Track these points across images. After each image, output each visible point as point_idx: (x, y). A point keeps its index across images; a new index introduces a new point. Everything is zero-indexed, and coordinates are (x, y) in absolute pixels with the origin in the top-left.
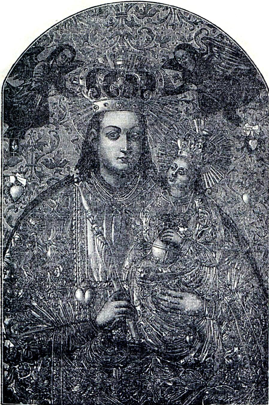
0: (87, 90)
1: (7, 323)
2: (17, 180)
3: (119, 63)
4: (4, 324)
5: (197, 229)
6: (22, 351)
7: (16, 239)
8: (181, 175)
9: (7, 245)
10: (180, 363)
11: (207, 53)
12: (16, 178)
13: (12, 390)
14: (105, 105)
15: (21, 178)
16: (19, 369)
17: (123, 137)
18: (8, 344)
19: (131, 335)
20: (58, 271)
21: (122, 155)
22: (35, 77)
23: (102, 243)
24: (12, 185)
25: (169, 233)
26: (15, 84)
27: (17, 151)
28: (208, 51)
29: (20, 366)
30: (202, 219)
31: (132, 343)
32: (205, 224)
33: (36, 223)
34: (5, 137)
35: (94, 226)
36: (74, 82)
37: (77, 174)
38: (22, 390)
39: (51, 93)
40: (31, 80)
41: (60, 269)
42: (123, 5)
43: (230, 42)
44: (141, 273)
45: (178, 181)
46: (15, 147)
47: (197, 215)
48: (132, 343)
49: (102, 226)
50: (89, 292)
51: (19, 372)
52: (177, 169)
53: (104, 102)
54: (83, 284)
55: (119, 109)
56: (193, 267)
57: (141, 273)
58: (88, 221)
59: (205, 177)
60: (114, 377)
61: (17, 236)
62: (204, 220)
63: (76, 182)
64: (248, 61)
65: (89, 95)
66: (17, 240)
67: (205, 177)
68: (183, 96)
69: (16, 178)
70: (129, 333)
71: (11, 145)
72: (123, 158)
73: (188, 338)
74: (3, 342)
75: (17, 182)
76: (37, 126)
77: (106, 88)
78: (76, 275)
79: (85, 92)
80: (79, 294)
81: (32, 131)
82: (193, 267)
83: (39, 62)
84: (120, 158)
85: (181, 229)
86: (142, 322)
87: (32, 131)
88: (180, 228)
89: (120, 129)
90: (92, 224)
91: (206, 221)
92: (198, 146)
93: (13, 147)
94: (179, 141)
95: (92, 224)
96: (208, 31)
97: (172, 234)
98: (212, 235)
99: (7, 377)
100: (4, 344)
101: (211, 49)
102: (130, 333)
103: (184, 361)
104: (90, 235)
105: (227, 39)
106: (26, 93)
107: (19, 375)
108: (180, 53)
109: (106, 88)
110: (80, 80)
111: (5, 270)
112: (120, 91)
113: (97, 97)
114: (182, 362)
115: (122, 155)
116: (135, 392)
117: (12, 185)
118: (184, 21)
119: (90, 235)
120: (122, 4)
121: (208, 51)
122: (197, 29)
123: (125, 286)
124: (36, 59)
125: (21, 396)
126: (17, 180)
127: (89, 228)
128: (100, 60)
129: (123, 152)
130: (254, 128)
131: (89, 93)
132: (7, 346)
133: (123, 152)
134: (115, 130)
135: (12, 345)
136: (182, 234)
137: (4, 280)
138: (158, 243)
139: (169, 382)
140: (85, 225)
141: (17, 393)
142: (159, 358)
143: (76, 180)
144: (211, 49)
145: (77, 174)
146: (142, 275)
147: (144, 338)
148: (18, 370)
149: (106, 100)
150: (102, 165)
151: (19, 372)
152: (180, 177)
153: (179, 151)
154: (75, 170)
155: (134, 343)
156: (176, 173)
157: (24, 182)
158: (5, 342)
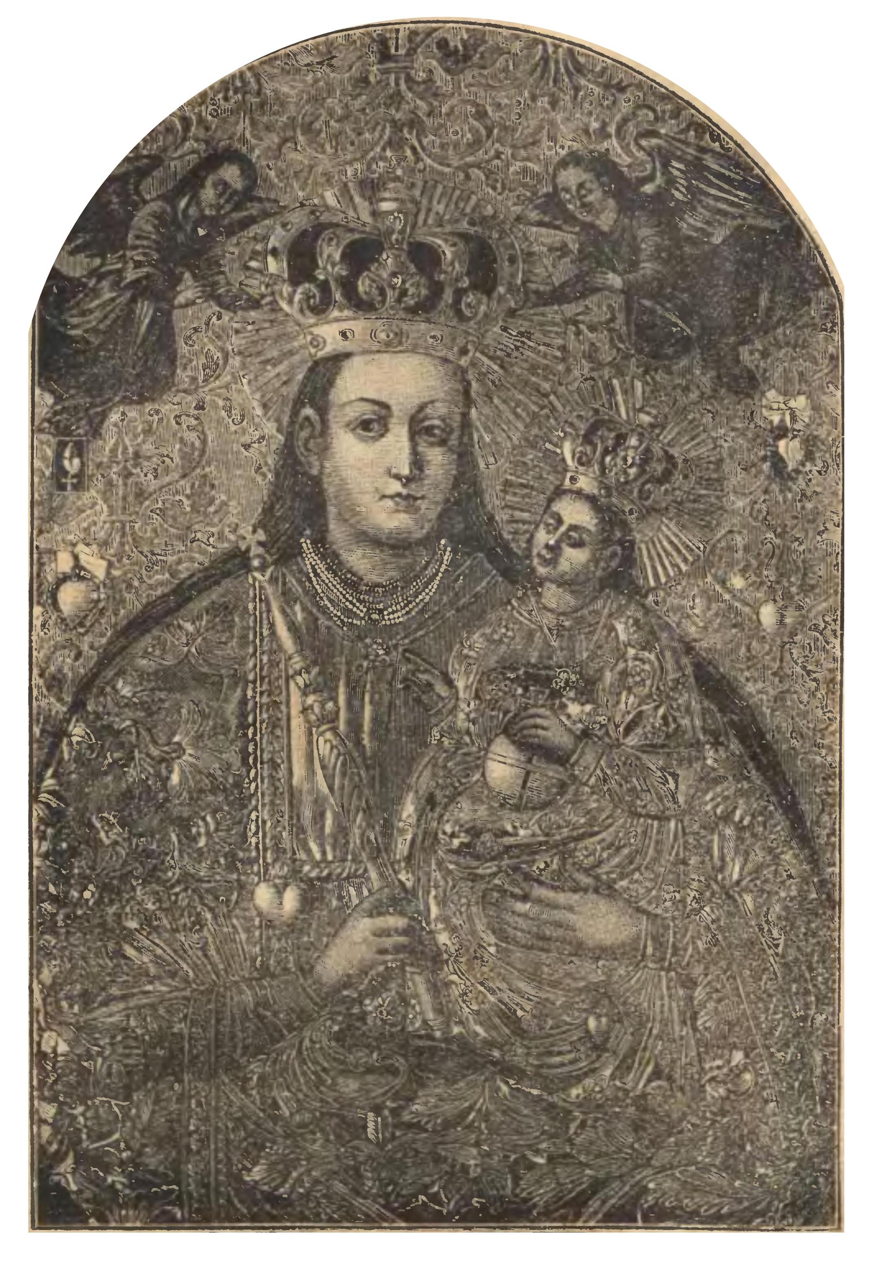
1: (48, 981)
3: (385, 206)
4: (40, 982)
7: (75, 739)
12: (76, 558)
13: (63, 1181)
14: (344, 334)
15: (92, 560)
16: (86, 1119)
18: (53, 1044)
19: (422, 1013)
20: (202, 830)
21: (396, 487)
22: (135, 247)
24: (64, 579)
25: (539, 721)
26: (77, 269)
27: (80, 475)
29: (88, 1108)
31: (420, 1037)
32: (647, 690)
34: (41, 430)
35: (310, 700)
36: (253, 264)
37: (260, 543)
38: (97, 1182)
39: (181, 299)
40: (124, 256)
41: (207, 824)
43: (722, 146)
44: (453, 835)
45: (564, 565)
46: (72, 465)
47: (621, 666)
48: (420, 1037)
49: (335, 700)
50: (298, 892)
51: (86, 1126)
52: (563, 529)
53: (344, 326)
54: (277, 866)
55: (388, 347)
56: (610, 821)
57: (453, 835)
58: (292, 685)
59: (645, 552)
61: (78, 730)
62: (643, 680)
63: (256, 569)
65: (296, 305)
69: (76, 558)
70: (414, 1007)
71: (59, 456)
72: (399, 495)
74: (36, 1038)
75: (78, 573)
76: (174, 723)
77: (348, 286)
78: (257, 844)
80: (263, 895)
83: (145, 202)
84: (392, 497)
85: (574, 709)
86: (454, 978)
87: (123, 414)
88: (569, 703)
89: (386, 406)
90: (305, 694)
91: (648, 682)
93: (66, 463)
95: (305, 694)
96: (654, 111)
97: (545, 723)
98: (666, 724)
99: (50, 1143)
100: (39, 1044)
102: (418, 1008)
105: (715, 138)
106: (108, 296)
107: (84, 1136)
108: (571, 177)
109: (348, 286)
110: (270, 259)
111: (42, 828)
112: (389, 293)
114: (575, 1092)
115: (396, 487)
116: (433, 1183)
117: (64, 579)
120: (397, 31)
121: (654, 169)
123: (403, 877)
125: (95, 1200)
126: (77, 565)
128: (330, 197)
129: (397, 477)
131: (297, 297)
132: (49, 1051)
133: (397, 477)
135: (63, 1048)
136: (574, 723)
137: (39, 856)
138: (502, 747)
139: (537, 1152)
140: (283, 697)
141: (80, 1192)
143: (256, 563)
145: (260, 543)
147: (461, 1023)
148: (81, 1119)
149: (348, 319)
151: (86, 1126)
154: (254, 531)
155: (431, 1037)
156: (558, 542)
157: (97, 567)
158: (41, 1036)
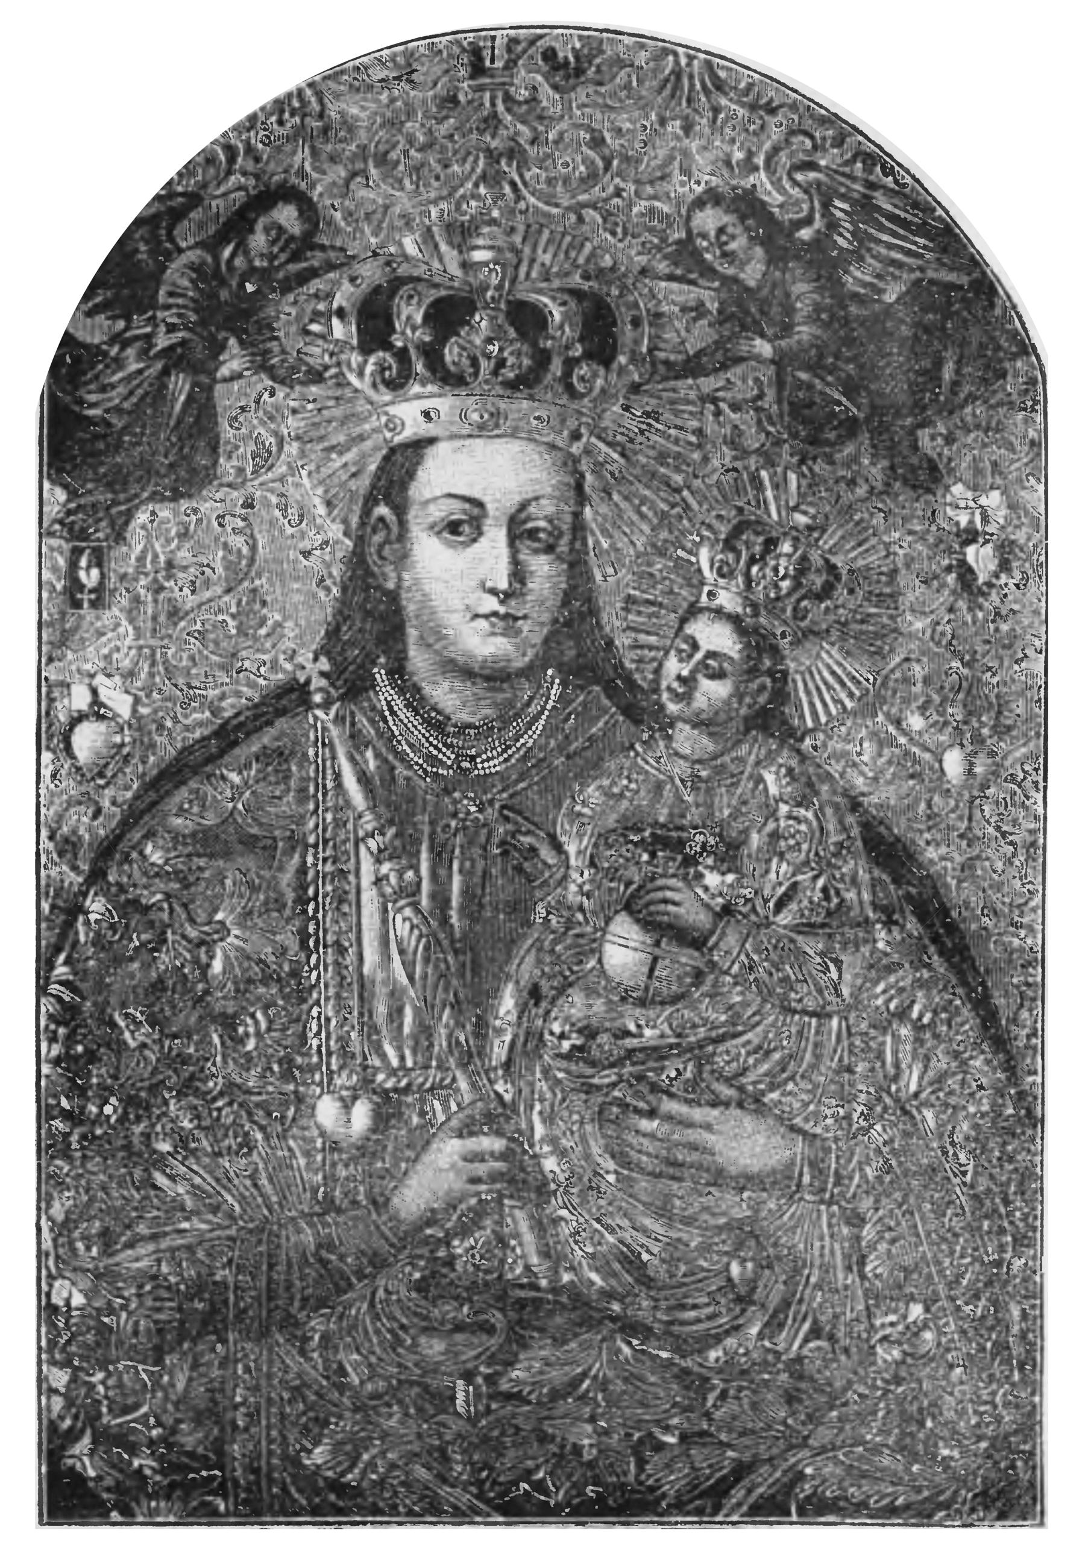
0: (360, 359)
1: (60, 1218)
2: (96, 700)
3: (479, 256)
5: (773, 876)
6: (119, 1317)
8: (712, 677)
9: (63, 936)
10: (706, 1359)
11: (808, 221)
12: (94, 692)
13: (78, 1465)
14: (427, 414)
15: (114, 694)
16: (107, 1388)
17: (495, 539)
18: (65, 1295)
19: (523, 1256)
20: (251, 1030)
21: (491, 604)
22: (168, 307)
23: (416, 932)
24: (79, 719)
26: (95, 334)
27: (99, 589)
28: (812, 209)
30: (792, 842)
33: (168, 859)
35: (385, 868)
37: (323, 674)
39: (224, 371)
41: (257, 1023)
42: (498, 42)
44: (562, 1036)
45: (700, 701)
46: (90, 578)
47: (771, 826)
48: (522, 1286)
50: (370, 1106)
51: (106, 1397)
52: (699, 656)
53: (427, 404)
54: (344, 1074)
56: (757, 1018)
57: (562, 1036)
58: (363, 849)
59: (800, 685)
60: (457, 1414)
61: (96, 906)
62: (798, 844)
64: (975, 263)
65: (367, 378)
66: (97, 921)
67: (800, 685)
68: (721, 384)
69: (94, 692)
70: (513, 1249)
71: (73, 565)
72: (495, 614)
73: (735, 1269)
74: (45, 1287)
75: (97, 710)
77: (432, 355)
79: (354, 365)
81: (153, 513)
82: (757, 1018)
83: (180, 251)
84: (486, 617)
85: (712, 879)
86: (564, 1213)
87: (153, 513)
88: (706, 872)
89: (479, 504)
90: (379, 861)
91: (805, 847)
92: (776, 570)
93: (82, 575)
94: (704, 554)
95: (379, 861)
98: (827, 898)
99: (62, 1418)
100: (48, 1295)
101: (826, 205)
102: (518, 1251)
103: (720, 1353)
104: (369, 898)
105: (888, 171)
107: (104, 1410)
108: (708, 220)
109: (432, 355)
110: (335, 321)
113: (396, 385)
114: (713, 1355)
115: (491, 604)
117: (79, 719)
118: (724, 102)
119: (369, 898)
120: (493, 38)
121: (812, 209)
122: (775, 134)
123: (500, 1087)
124: (171, 239)
125: (118, 1488)
126: (96, 700)
127: (366, 880)
128: (410, 245)
129: (493, 592)
130: (983, 501)
133: (493, 592)
134: (465, 512)
136: (713, 896)
137: (48, 1061)
138: (623, 927)
139: (667, 1429)
140: (351, 865)
141: (99, 1478)
142: (629, 1344)
143: (318, 698)
144: (826, 205)
145: (323, 674)
146: (566, 1045)
147: (572, 1268)
148: (101, 1389)
149: (432, 396)
150: (412, 633)
151: (106, 1397)
152: (707, 685)
153: (706, 589)
154: (316, 659)
155: (535, 1287)
156: (693, 672)
157: (121, 704)
158: (51, 1286)
